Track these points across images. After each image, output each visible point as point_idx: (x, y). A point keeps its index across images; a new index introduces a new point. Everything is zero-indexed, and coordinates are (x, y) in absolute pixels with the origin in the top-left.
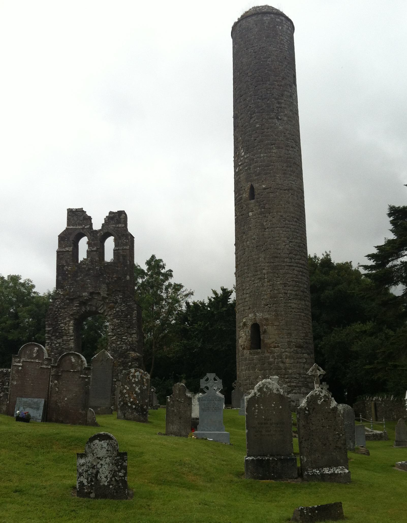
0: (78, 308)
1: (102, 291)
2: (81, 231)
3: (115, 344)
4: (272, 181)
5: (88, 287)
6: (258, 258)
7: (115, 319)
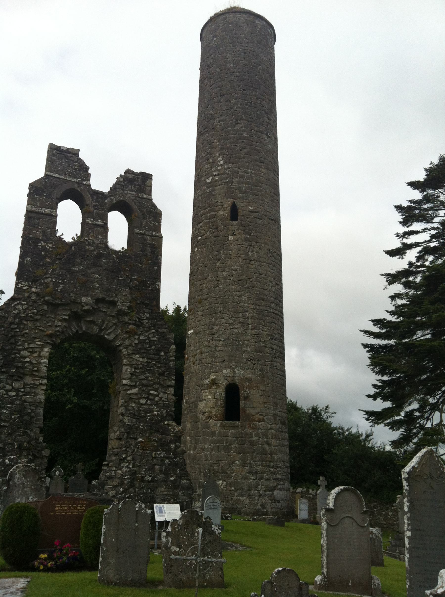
0: (65, 324)
1: (121, 299)
2: (76, 186)
3: (135, 402)
4: (261, 205)
5: (94, 288)
6: (240, 296)
7: (138, 356)
